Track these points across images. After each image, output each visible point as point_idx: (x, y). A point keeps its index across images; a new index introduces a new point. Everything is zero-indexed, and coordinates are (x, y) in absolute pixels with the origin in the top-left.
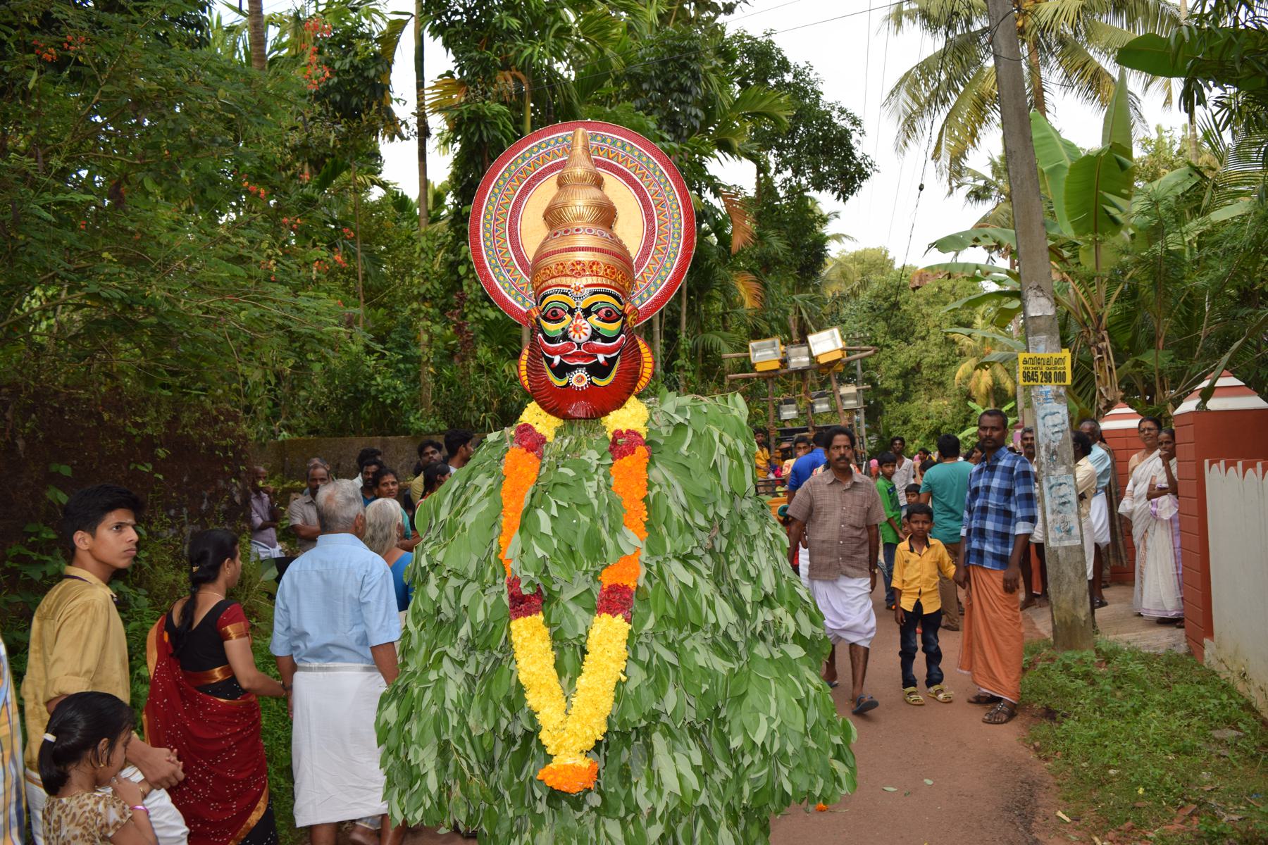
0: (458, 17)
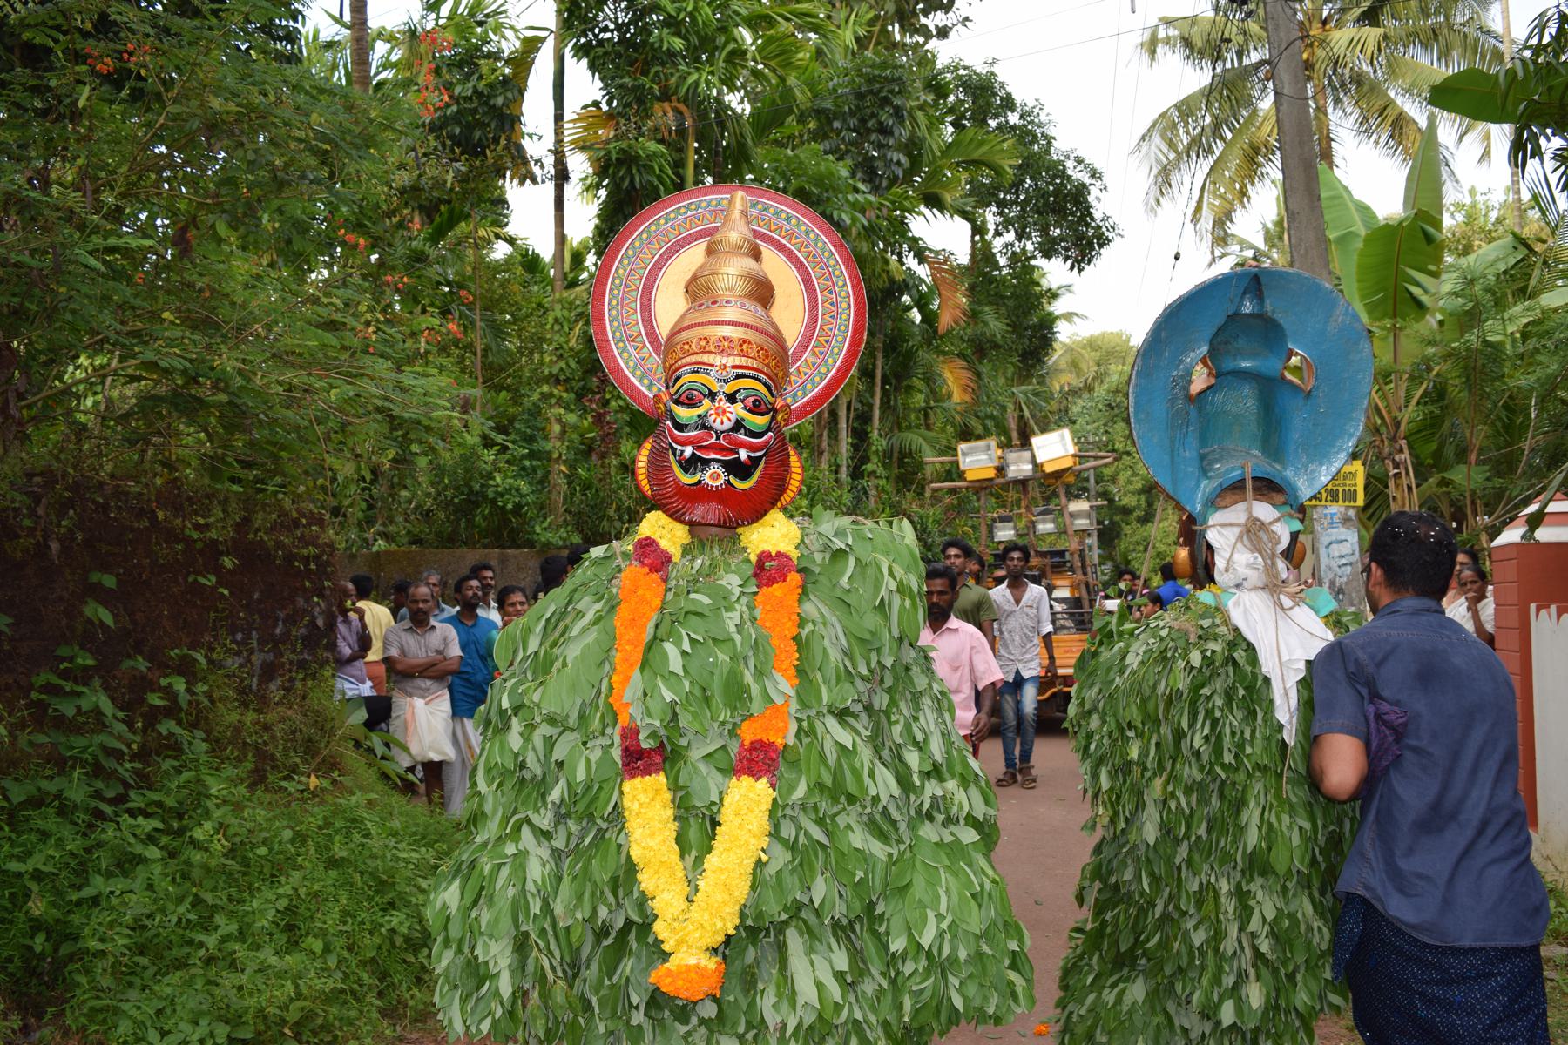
0: (608, 35)
